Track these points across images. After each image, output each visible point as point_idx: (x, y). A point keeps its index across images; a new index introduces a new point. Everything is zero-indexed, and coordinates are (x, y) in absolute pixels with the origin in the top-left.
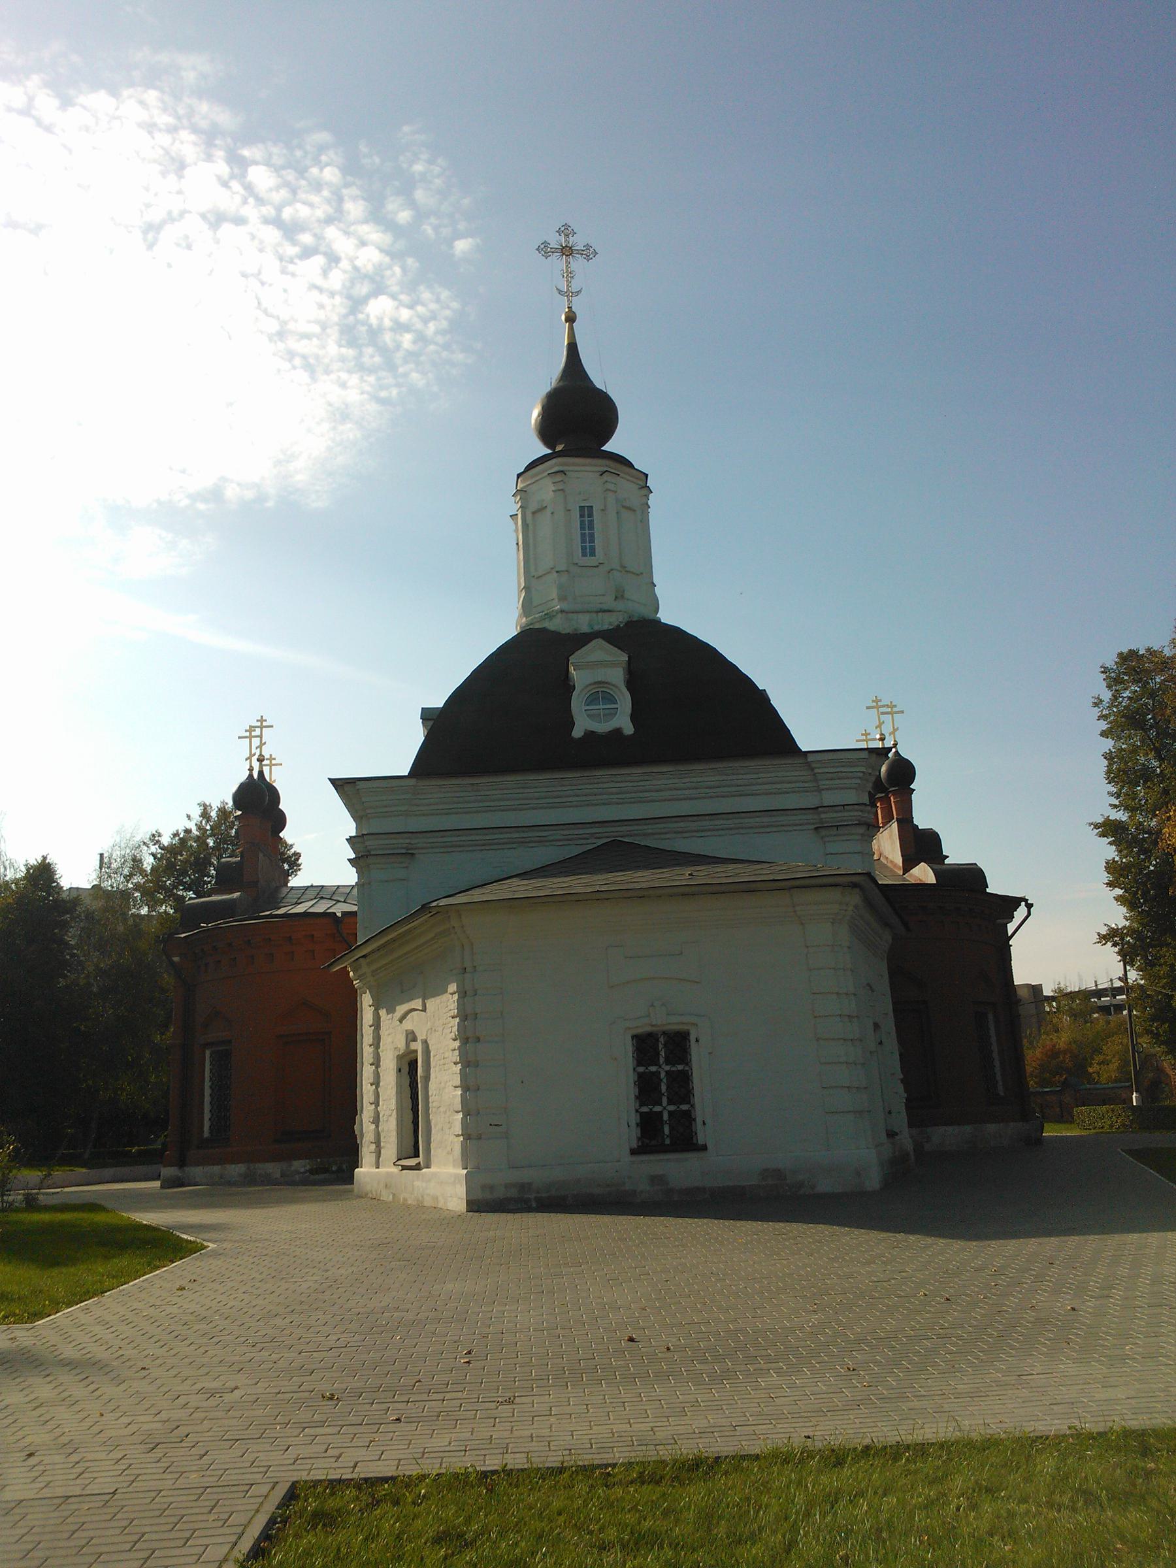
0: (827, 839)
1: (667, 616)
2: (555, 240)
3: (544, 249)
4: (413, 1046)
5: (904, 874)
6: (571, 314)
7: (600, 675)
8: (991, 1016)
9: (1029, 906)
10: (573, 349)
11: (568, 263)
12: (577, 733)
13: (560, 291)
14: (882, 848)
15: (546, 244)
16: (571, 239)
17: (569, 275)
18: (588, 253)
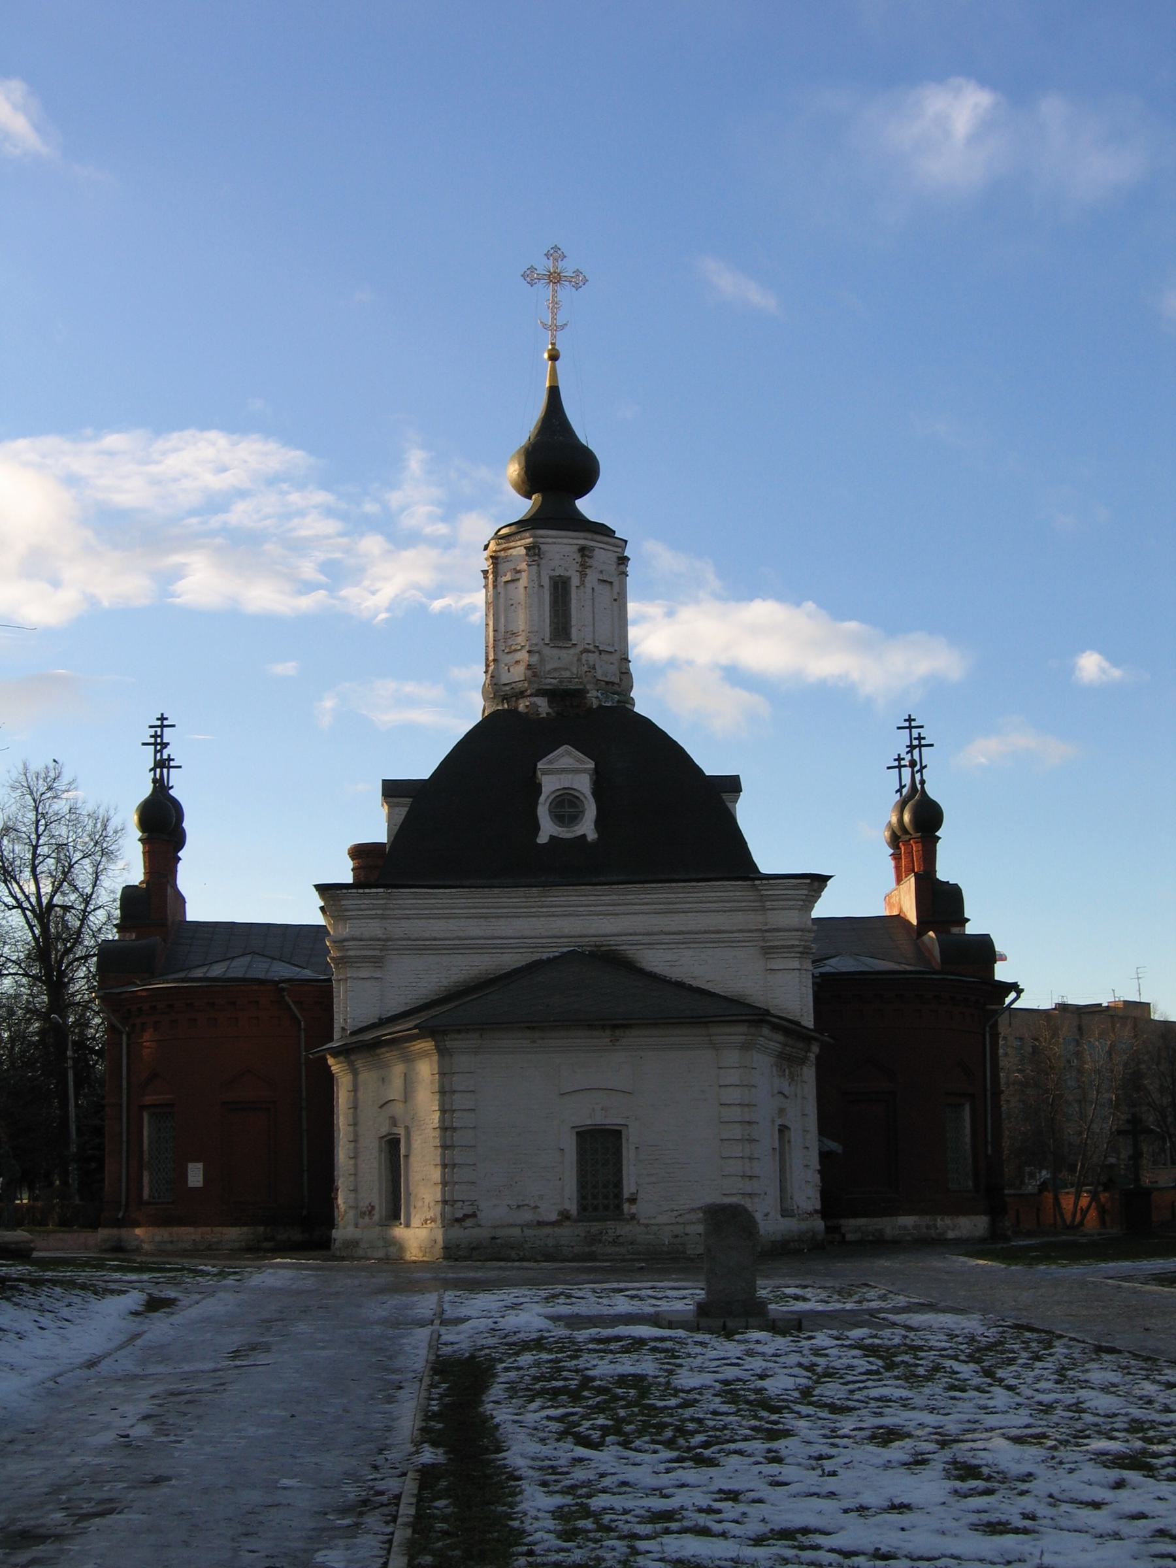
0: (767, 956)
1: (640, 708)
2: (544, 265)
3: (530, 276)
4: (395, 1130)
5: (917, 939)
6: (554, 353)
7: (565, 781)
8: (967, 1108)
9: (1019, 992)
10: (554, 393)
11: (555, 291)
12: (543, 839)
13: (544, 326)
14: (902, 902)
15: (532, 269)
16: (560, 264)
17: (555, 305)
18: (579, 281)
